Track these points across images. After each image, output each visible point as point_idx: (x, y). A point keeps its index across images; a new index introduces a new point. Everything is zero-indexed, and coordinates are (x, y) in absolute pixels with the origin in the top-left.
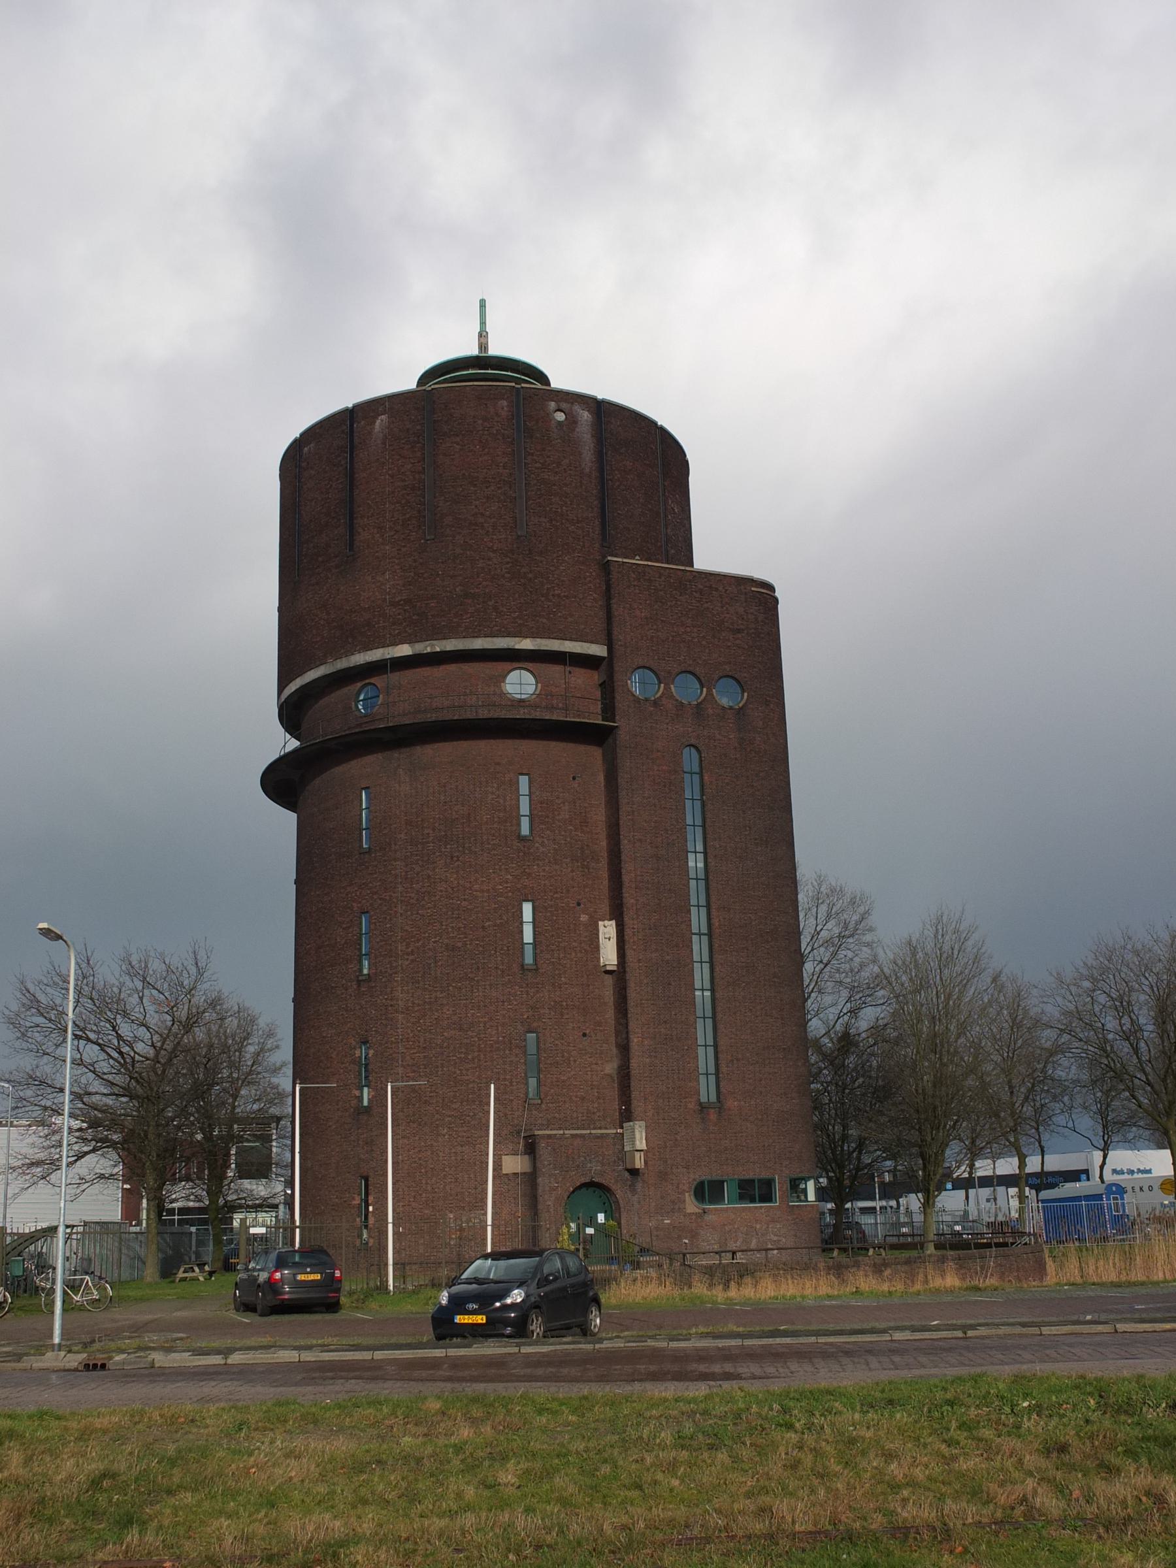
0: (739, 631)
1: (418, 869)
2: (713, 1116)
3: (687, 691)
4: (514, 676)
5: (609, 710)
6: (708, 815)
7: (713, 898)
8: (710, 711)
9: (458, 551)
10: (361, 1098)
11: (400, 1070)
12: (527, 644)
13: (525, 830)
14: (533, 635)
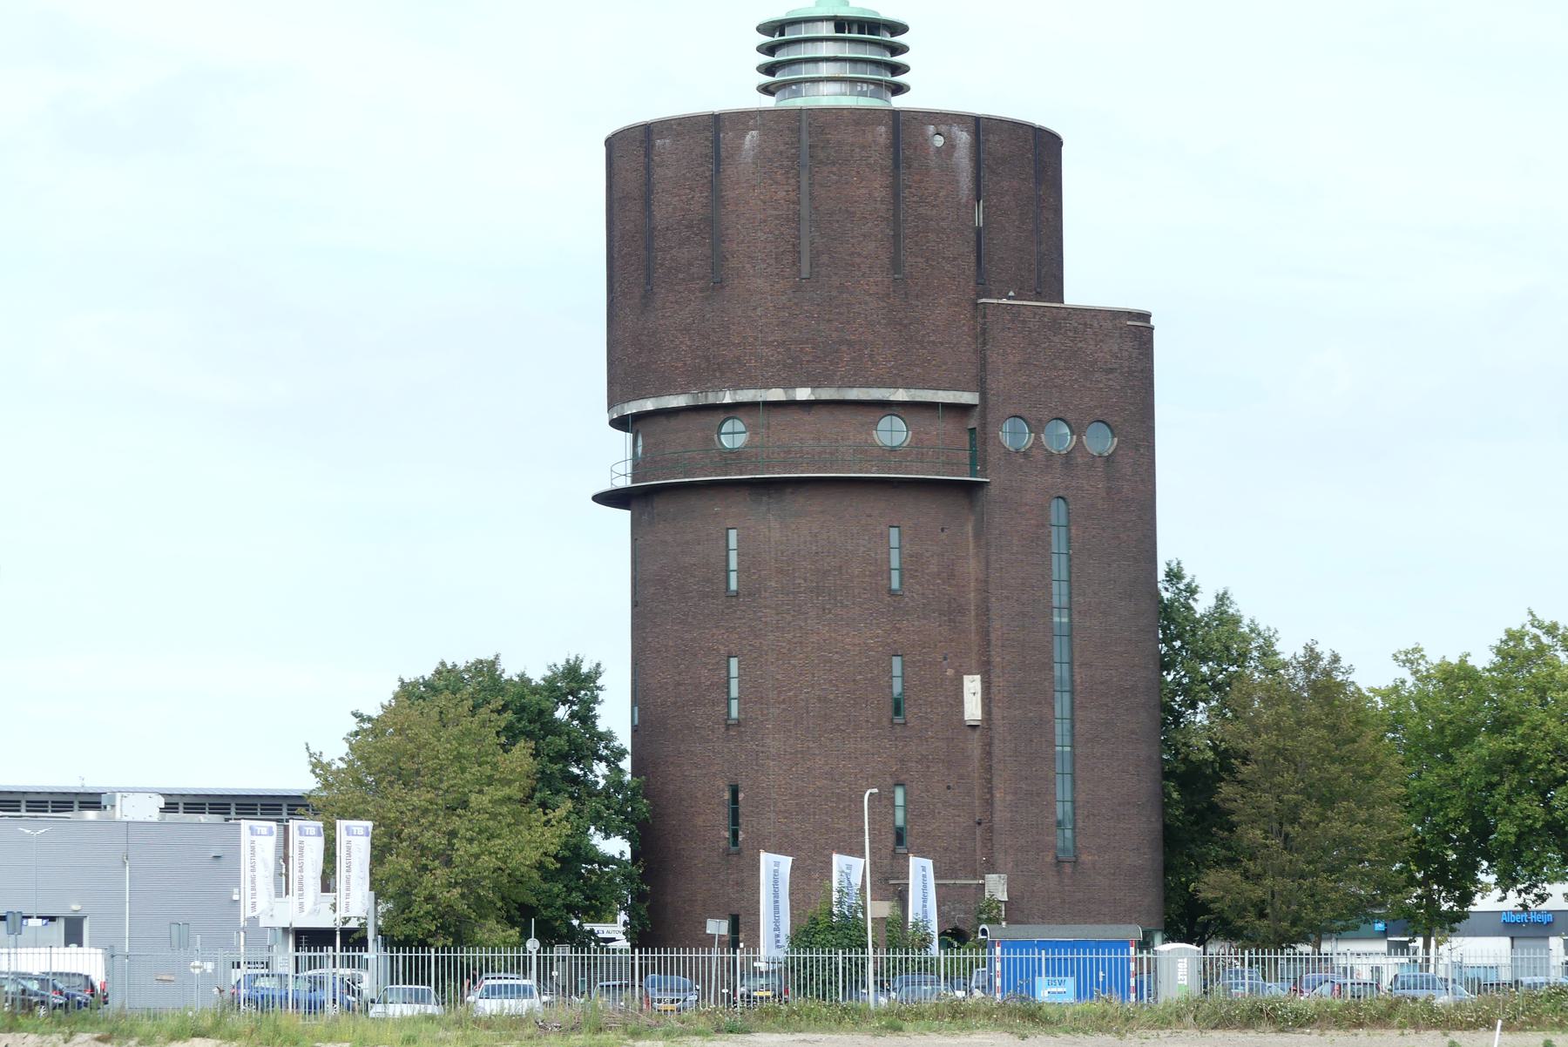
0: (1111, 371)
1: (789, 618)
2: (1068, 869)
3: (1060, 438)
4: (885, 423)
5: (977, 460)
6: (1075, 570)
7: (1077, 654)
8: (1079, 460)
9: (834, 293)
11: (772, 815)
12: (901, 395)
13: (895, 584)
14: (907, 386)
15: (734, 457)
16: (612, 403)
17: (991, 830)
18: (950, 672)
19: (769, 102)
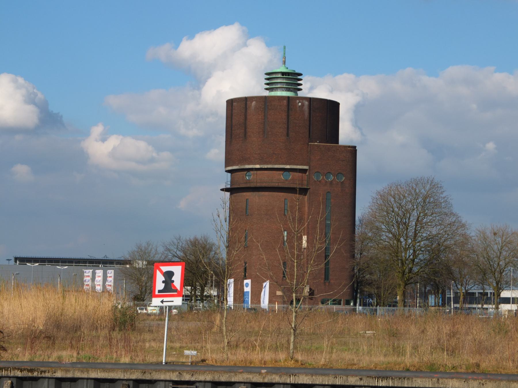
14: (289, 165)
15: (249, 181)
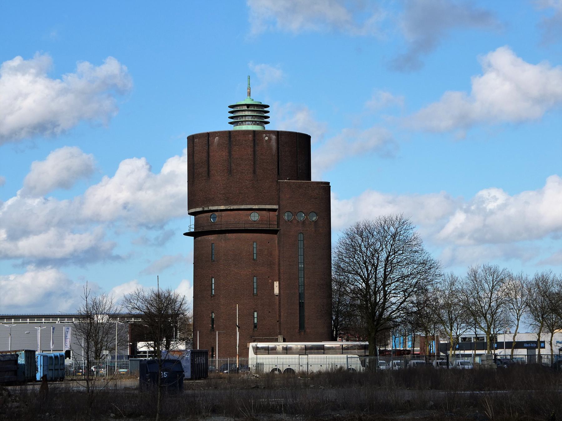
0: (316, 198)
4: (253, 214)
10: (212, 316)
14: (258, 204)
16: (189, 209)
17: (280, 323)
18: (270, 281)
19: (232, 128)
